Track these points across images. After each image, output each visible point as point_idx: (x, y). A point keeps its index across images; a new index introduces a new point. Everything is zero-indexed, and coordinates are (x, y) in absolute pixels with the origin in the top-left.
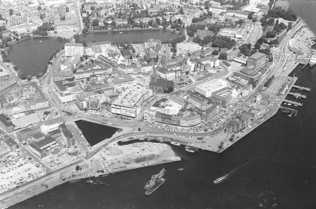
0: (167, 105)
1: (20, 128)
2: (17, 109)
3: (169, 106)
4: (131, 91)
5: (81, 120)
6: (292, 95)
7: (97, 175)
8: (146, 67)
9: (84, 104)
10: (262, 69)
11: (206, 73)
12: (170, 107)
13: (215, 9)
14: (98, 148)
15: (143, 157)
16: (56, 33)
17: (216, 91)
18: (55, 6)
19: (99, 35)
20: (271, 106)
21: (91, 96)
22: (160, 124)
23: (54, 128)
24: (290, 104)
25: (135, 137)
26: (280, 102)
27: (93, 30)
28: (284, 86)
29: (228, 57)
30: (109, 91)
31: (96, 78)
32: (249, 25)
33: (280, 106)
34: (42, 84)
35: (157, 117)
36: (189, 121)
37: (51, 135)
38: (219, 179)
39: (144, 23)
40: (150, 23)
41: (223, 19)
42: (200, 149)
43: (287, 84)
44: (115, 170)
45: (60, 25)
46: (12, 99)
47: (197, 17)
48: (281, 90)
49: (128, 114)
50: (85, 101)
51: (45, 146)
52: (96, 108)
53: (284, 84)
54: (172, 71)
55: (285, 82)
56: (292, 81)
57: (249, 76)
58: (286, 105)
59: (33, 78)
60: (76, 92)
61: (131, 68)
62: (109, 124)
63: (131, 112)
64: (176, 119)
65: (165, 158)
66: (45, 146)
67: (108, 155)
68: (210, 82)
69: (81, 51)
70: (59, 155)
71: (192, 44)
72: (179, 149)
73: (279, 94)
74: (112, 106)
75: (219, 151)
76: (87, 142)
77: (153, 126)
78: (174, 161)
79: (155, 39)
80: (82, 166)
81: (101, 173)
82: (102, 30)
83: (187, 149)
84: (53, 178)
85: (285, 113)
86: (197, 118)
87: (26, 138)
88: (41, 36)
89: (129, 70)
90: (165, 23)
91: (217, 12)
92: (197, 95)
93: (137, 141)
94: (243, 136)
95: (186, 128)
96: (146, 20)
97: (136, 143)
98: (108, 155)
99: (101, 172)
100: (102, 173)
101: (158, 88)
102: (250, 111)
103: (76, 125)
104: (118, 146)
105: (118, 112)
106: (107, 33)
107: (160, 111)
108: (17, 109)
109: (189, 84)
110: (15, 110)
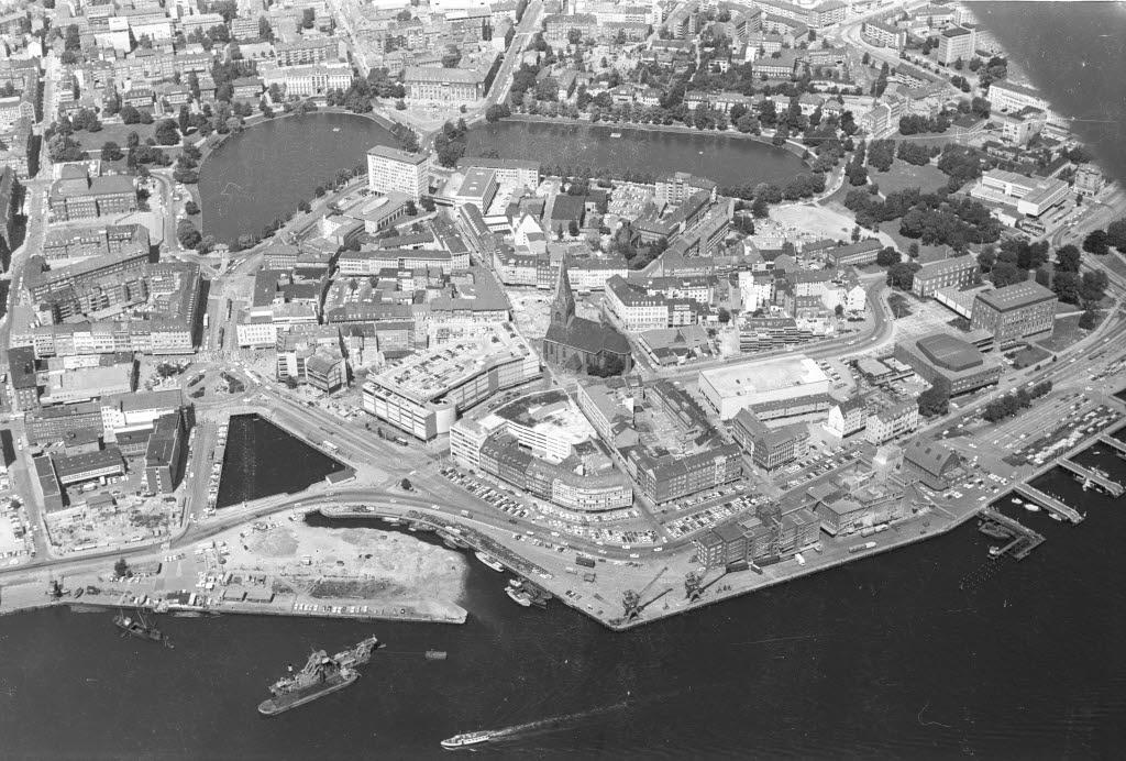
0: (548, 418)
1: (58, 400)
2: (87, 340)
3: (555, 422)
4: (460, 346)
5: (255, 415)
6: (1072, 473)
7: (163, 606)
8: (584, 272)
9: (288, 362)
10: (1029, 348)
11: (781, 327)
12: (556, 427)
13: (1012, 93)
14: (235, 519)
15: (348, 580)
16: (401, 107)
17: (770, 403)
18: (449, 16)
19: (546, 135)
20: (950, 497)
21: (320, 341)
22: (489, 478)
23: (142, 424)
24: (1035, 508)
25: (373, 508)
26: (996, 491)
27: (527, 114)
28: (1062, 432)
29: (917, 283)
30: (397, 333)
31: (395, 280)
32: (1093, 170)
33: (984, 506)
34: (1118, 414)
35: (490, 456)
36: (582, 491)
37: (122, 443)
38: (467, 738)
39: (720, 110)
40: (738, 112)
41: (1018, 136)
42: (556, 601)
43: (1082, 427)
44: (228, 603)
45: (424, 82)
46: (105, 307)
47: (920, 114)
48: (1038, 446)
49: (406, 423)
50: (292, 351)
51: (81, 476)
52: (323, 384)
53: (1071, 425)
54: (659, 299)
55: (1083, 417)
56: (1114, 416)
57: (936, 367)
58: (1017, 505)
59: (217, 246)
60: (291, 318)
61: (528, 266)
62: (328, 447)
63: (415, 418)
64: (542, 474)
65: (414, 604)
66: (81, 476)
67: (246, 548)
68: (766, 364)
69: (416, 183)
70: (103, 515)
71: (838, 211)
72: (484, 584)
73: (1017, 461)
74: (367, 386)
75: (619, 621)
76: (216, 490)
77: (463, 483)
78: (438, 619)
79: (698, 172)
80: (137, 566)
81: (176, 604)
82: (560, 116)
83: (513, 587)
84: (34, 580)
85: (986, 535)
86: (617, 485)
87: (49, 438)
88: (351, 112)
89: (520, 270)
90: (793, 121)
91: (1013, 105)
92: (680, 404)
93: (376, 523)
94: (748, 589)
95: (568, 516)
96: (723, 102)
97: (361, 529)
98: (246, 548)
99: (177, 601)
100: (180, 603)
101: (571, 351)
102: (831, 498)
103: (225, 429)
104: (305, 525)
105: (381, 409)
106: (575, 130)
107: (516, 434)
108: (87, 340)
109: (703, 359)
110: (80, 340)
